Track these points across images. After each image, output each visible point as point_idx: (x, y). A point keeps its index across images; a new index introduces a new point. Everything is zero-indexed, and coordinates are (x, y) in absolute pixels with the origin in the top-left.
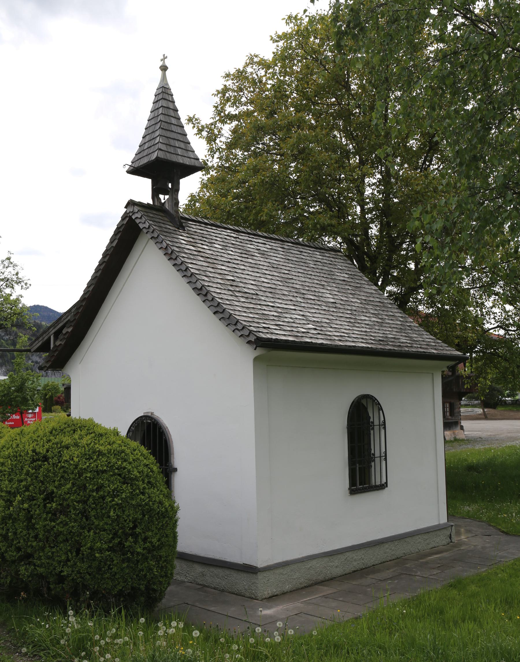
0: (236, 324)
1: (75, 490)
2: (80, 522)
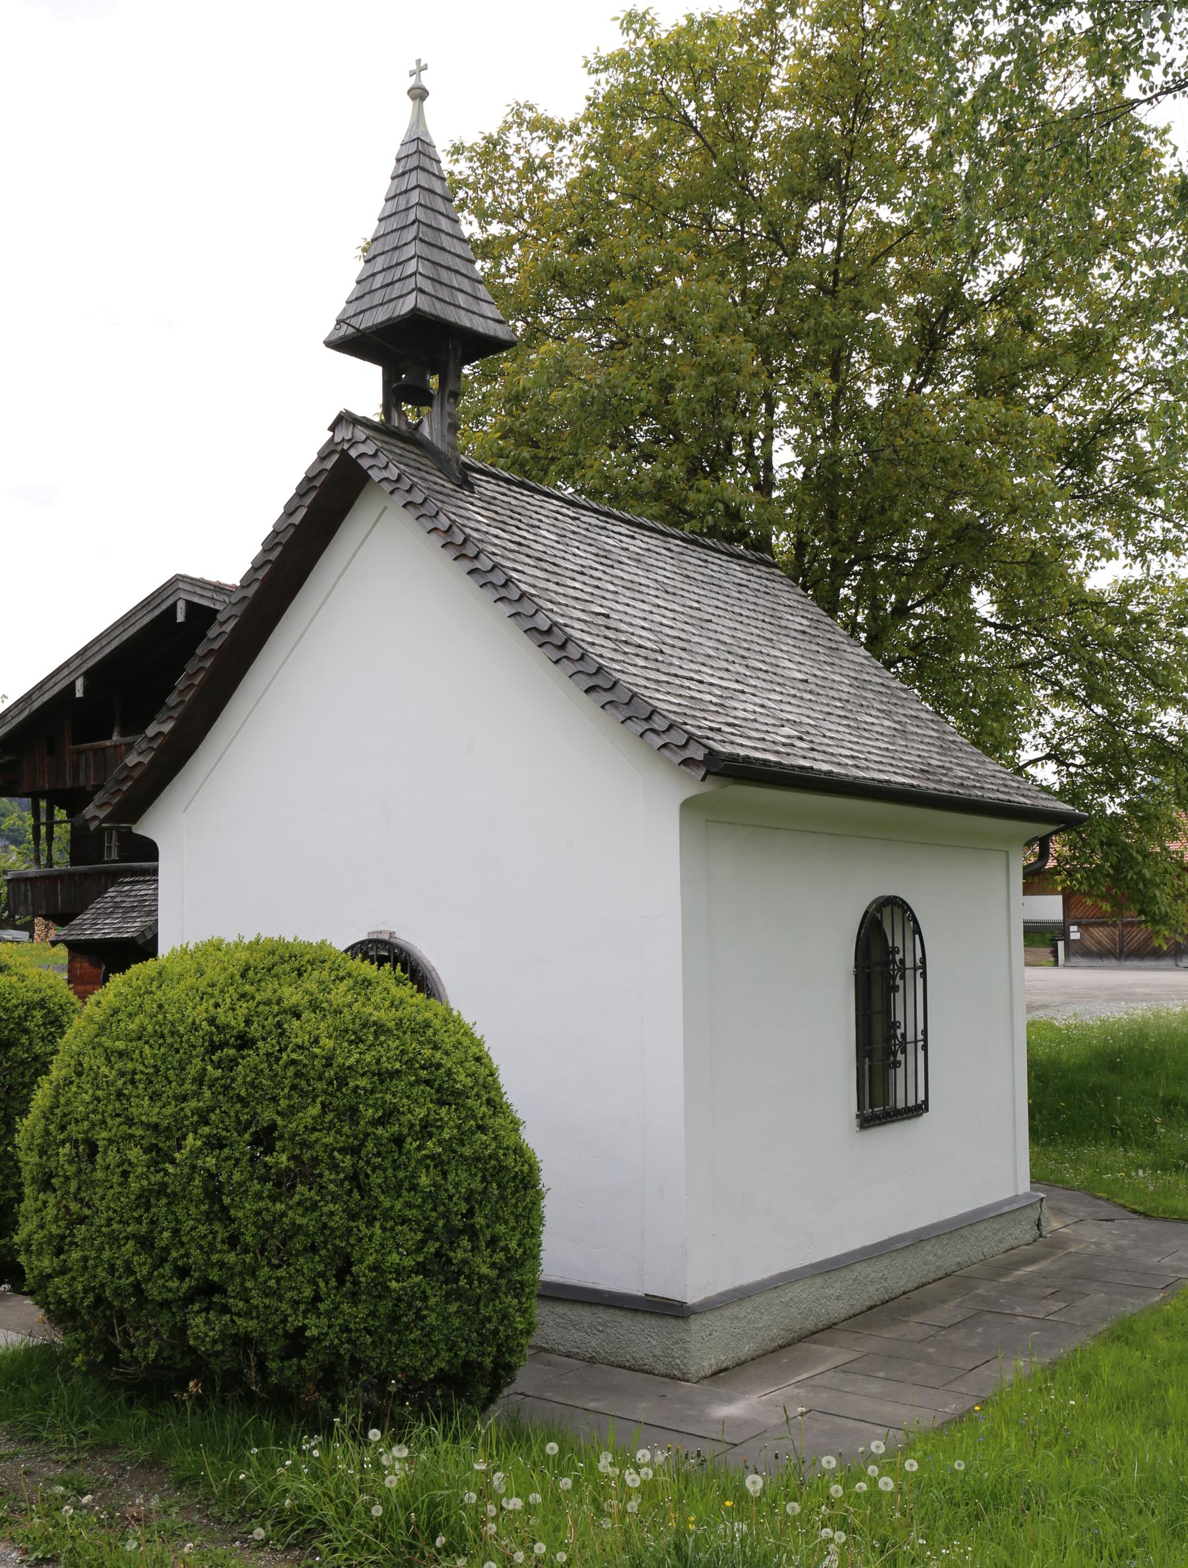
0: (648, 719)
1: (331, 1122)
2: (346, 1203)
